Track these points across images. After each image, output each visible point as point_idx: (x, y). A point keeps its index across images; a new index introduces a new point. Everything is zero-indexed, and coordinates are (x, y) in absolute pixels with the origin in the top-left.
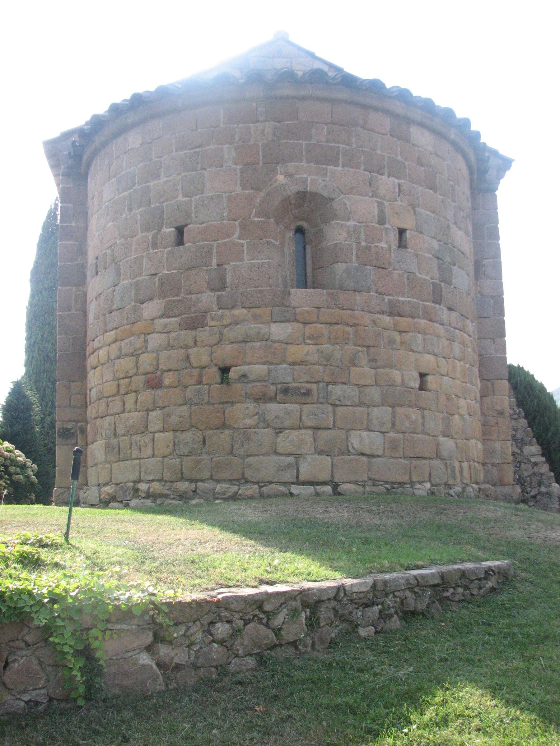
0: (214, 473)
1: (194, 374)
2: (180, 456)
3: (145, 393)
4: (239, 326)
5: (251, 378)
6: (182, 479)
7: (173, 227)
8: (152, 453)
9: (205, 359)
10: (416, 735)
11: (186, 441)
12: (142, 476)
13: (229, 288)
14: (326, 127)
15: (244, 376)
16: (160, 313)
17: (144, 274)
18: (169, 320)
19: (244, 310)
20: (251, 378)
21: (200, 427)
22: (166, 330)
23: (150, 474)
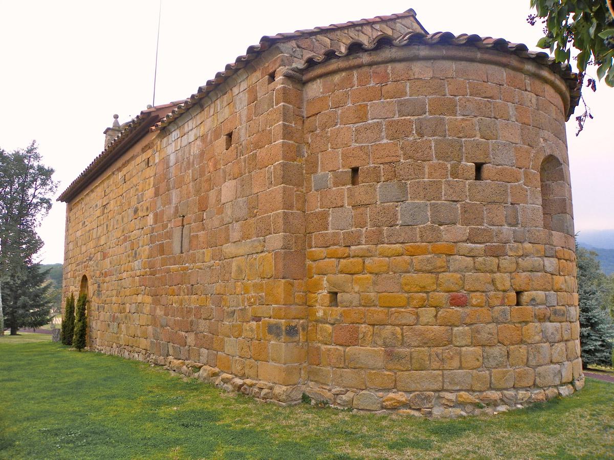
0: (516, 382)
1: (499, 296)
2: (488, 369)
3: (448, 310)
4: (528, 258)
5: (538, 301)
6: (491, 388)
7: (473, 163)
8: (459, 365)
9: (508, 285)
10: (140, 433)
11: (495, 355)
12: (445, 386)
13: (520, 225)
14: (408, 84)
15: (533, 300)
16: (465, 238)
17: (443, 198)
18: (473, 245)
19: (530, 244)
20: (538, 301)
21: (505, 343)
22: (472, 254)
23: (457, 384)
